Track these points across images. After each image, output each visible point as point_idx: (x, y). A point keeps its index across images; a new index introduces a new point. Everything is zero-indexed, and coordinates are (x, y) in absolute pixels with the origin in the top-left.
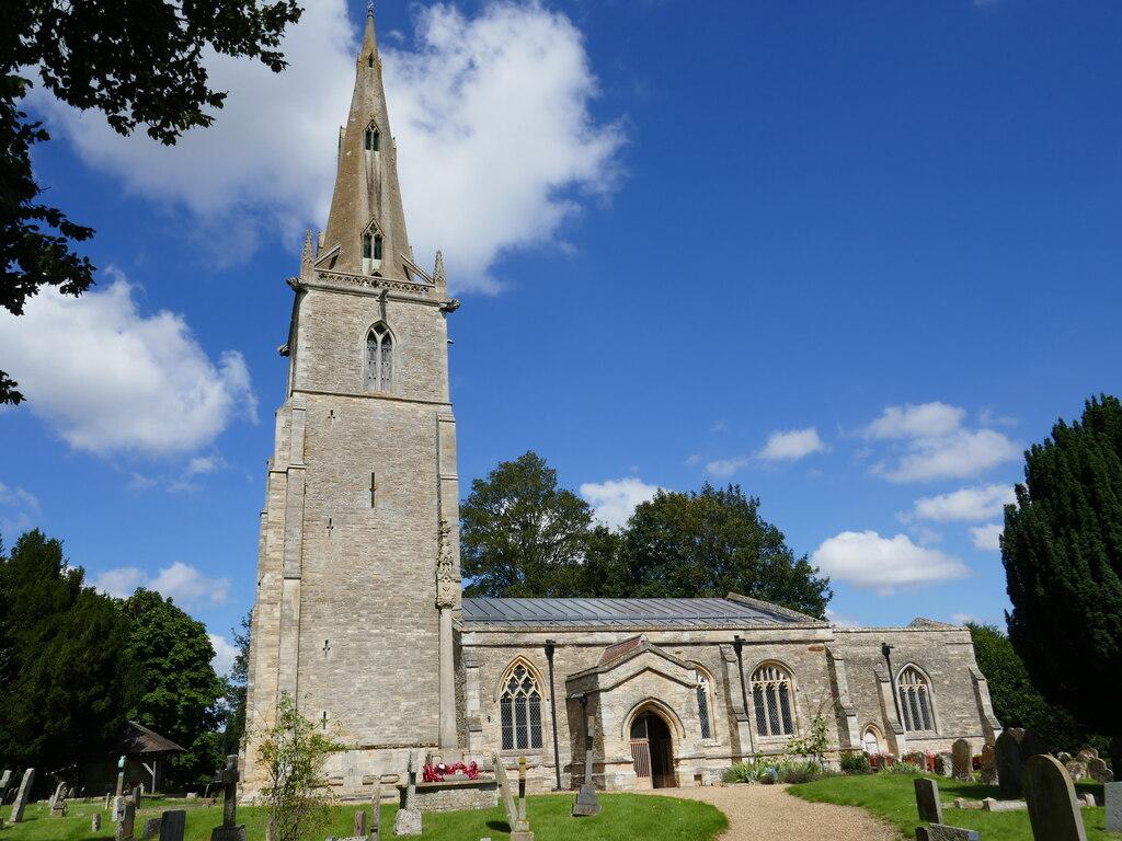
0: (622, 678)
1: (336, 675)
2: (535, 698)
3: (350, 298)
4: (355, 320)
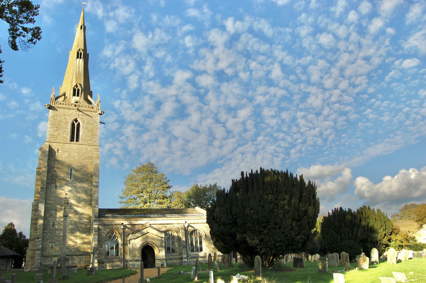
3: (67, 110)
4: (68, 118)
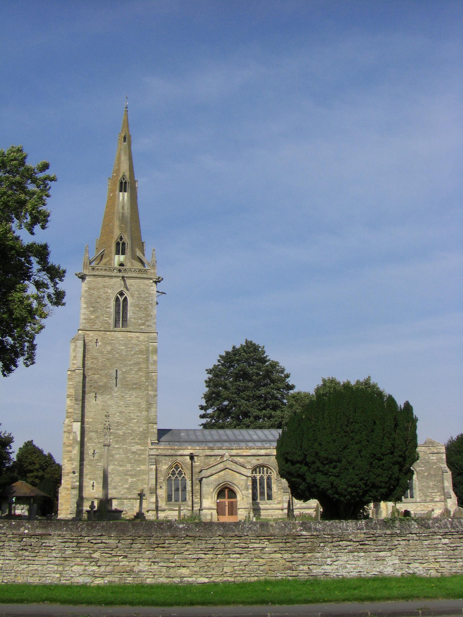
0: (214, 472)
1: (99, 465)
2: (184, 479)
3: (107, 279)
4: (109, 291)
